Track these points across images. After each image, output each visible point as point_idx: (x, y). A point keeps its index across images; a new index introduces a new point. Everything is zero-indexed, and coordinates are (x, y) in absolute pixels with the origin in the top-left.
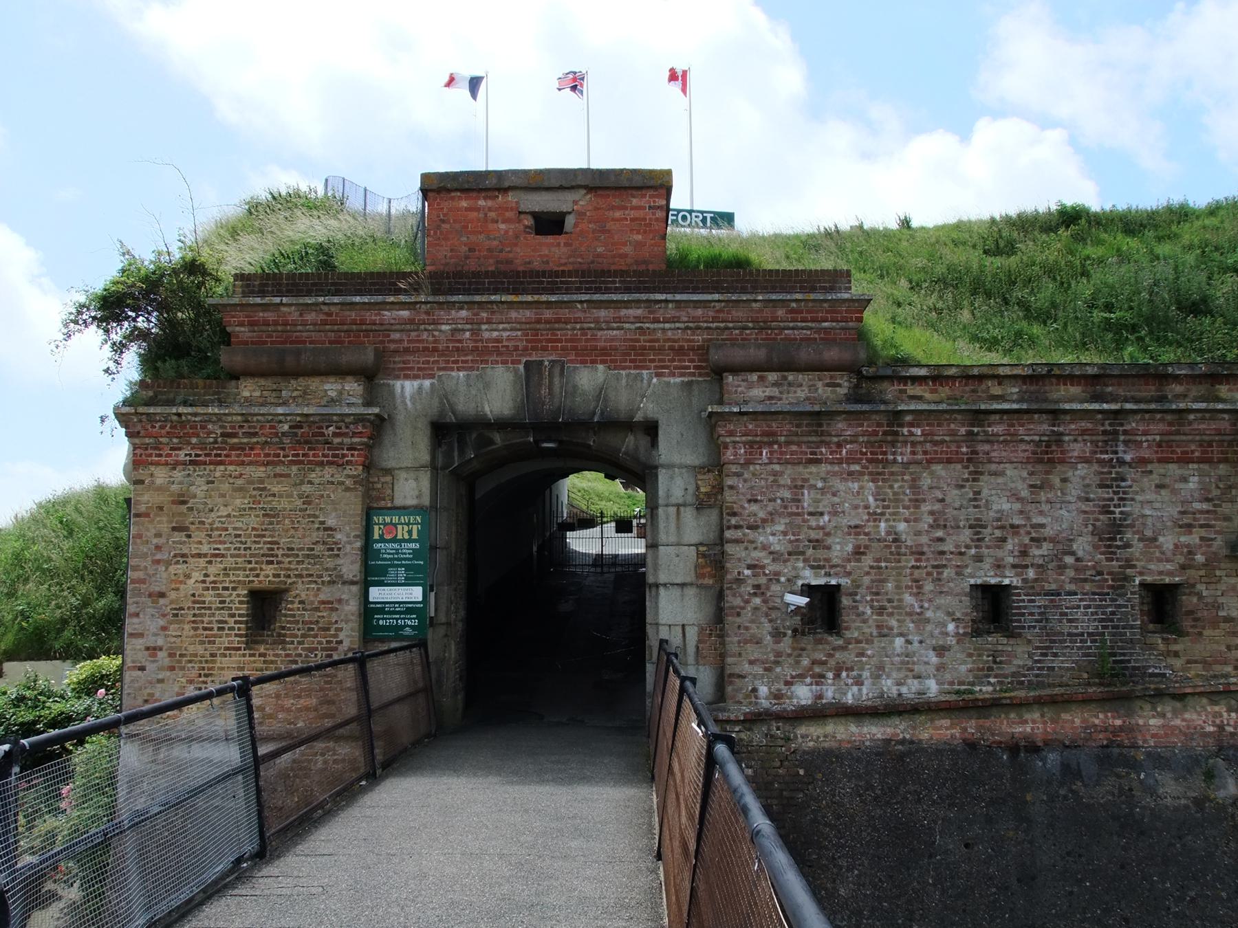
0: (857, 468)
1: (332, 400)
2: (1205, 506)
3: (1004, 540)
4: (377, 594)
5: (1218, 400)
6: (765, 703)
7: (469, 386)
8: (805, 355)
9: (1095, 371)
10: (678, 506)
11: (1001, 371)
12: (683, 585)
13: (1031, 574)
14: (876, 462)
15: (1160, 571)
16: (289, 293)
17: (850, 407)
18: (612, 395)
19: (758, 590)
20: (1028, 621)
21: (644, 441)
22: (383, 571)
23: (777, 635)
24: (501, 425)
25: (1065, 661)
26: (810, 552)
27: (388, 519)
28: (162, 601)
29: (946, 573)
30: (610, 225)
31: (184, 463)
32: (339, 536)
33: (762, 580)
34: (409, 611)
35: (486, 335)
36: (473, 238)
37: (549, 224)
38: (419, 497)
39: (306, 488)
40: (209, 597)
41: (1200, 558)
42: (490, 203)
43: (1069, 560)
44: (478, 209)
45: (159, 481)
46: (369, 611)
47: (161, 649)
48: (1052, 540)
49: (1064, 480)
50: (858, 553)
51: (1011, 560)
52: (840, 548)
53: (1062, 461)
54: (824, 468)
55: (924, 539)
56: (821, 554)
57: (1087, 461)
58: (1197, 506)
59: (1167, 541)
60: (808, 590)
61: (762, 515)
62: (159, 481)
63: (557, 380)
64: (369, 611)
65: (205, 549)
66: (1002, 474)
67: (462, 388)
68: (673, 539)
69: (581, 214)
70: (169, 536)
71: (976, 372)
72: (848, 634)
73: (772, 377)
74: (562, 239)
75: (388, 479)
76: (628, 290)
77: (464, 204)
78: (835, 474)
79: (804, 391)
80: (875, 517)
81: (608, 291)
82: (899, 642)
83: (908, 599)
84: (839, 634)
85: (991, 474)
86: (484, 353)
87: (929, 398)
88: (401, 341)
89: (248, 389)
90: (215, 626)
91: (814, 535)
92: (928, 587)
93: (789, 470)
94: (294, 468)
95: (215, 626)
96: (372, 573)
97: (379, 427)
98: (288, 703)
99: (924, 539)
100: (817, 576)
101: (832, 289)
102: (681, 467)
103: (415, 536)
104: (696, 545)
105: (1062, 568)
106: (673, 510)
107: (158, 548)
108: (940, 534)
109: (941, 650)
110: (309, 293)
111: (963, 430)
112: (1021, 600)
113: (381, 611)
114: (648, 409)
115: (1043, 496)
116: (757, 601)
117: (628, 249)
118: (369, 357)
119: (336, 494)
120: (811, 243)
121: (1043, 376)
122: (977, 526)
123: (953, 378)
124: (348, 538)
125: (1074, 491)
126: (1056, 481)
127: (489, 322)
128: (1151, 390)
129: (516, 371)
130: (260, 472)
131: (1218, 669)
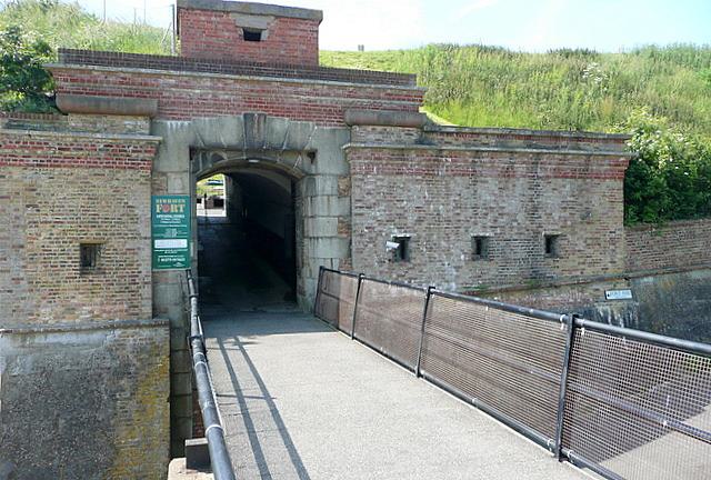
0: (420, 177)
1: (130, 130)
2: (572, 199)
3: (487, 214)
4: (159, 244)
5: (580, 149)
6: (375, 297)
7: (211, 125)
8: (397, 118)
9: (530, 133)
10: (328, 196)
11: (489, 131)
12: (331, 238)
13: (498, 231)
14: (429, 174)
15: (549, 230)
16: (96, 63)
17: (415, 146)
18: (293, 135)
19: (372, 240)
20: (496, 253)
21: (307, 160)
22: (163, 230)
23: (381, 262)
24: (229, 149)
25: (512, 272)
26: (397, 220)
27: (165, 201)
28: (21, 250)
29: (462, 230)
30: (288, 39)
31: (33, 166)
32: (137, 212)
33: (374, 235)
34: (179, 253)
35: (221, 97)
36: (209, 39)
37: (252, 36)
38: (183, 189)
39: (116, 183)
40: (54, 247)
41: (569, 223)
42: (218, 19)
43: (515, 224)
44: (211, 22)
45: (15, 177)
46: (155, 253)
47: (22, 279)
48: (508, 214)
49: (514, 186)
50: (420, 221)
51: (490, 224)
52: (411, 218)
53: (513, 176)
54: (404, 177)
55: (451, 214)
56: (403, 221)
57: (524, 176)
58: (569, 199)
59: (556, 215)
60: (396, 239)
61: (373, 201)
62: (15, 177)
63: (262, 125)
64: (155, 253)
65: (50, 218)
66: (487, 182)
67: (208, 127)
68: (326, 214)
69: (272, 31)
70: (24, 211)
71: (477, 131)
72: (413, 261)
73: (379, 128)
74: (261, 44)
75: (164, 178)
76: (302, 77)
77: (203, 18)
78: (409, 181)
79: (396, 136)
80: (428, 203)
81: (290, 76)
82: (439, 264)
83: (443, 243)
84: (409, 261)
85: (482, 182)
86: (219, 107)
87: (455, 145)
88: (169, 97)
89: (73, 121)
90: (59, 264)
91: (399, 211)
92: (453, 238)
93: (387, 178)
94: (107, 170)
95: (59, 264)
96: (157, 232)
97: (158, 149)
98: (108, 308)
99: (451, 214)
100: (400, 232)
101: (407, 84)
102: (330, 175)
103: (181, 211)
104: (338, 217)
105: (512, 228)
106: (326, 198)
107: (17, 218)
108: (458, 211)
109: (457, 268)
110: (109, 64)
111: (471, 160)
112: (493, 244)
113: (163, 253)
114: (312, 144)
115: (505, 193)
116: (371, 245)
117: (298, 53)
118: (153, 105)
119: (136, 186)
120: (390, 57)
121: (506, 135)
122: (475, 207)
123: (466, 133)
124: (143, 211)
125: (518, 190)
126: (510, 185)
127: (223, 89)
128: (553, 143)
129: (239, 118)
130: (84, 172)
131: (574, 274)
